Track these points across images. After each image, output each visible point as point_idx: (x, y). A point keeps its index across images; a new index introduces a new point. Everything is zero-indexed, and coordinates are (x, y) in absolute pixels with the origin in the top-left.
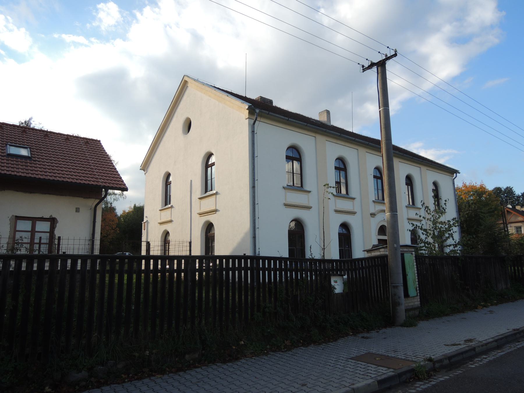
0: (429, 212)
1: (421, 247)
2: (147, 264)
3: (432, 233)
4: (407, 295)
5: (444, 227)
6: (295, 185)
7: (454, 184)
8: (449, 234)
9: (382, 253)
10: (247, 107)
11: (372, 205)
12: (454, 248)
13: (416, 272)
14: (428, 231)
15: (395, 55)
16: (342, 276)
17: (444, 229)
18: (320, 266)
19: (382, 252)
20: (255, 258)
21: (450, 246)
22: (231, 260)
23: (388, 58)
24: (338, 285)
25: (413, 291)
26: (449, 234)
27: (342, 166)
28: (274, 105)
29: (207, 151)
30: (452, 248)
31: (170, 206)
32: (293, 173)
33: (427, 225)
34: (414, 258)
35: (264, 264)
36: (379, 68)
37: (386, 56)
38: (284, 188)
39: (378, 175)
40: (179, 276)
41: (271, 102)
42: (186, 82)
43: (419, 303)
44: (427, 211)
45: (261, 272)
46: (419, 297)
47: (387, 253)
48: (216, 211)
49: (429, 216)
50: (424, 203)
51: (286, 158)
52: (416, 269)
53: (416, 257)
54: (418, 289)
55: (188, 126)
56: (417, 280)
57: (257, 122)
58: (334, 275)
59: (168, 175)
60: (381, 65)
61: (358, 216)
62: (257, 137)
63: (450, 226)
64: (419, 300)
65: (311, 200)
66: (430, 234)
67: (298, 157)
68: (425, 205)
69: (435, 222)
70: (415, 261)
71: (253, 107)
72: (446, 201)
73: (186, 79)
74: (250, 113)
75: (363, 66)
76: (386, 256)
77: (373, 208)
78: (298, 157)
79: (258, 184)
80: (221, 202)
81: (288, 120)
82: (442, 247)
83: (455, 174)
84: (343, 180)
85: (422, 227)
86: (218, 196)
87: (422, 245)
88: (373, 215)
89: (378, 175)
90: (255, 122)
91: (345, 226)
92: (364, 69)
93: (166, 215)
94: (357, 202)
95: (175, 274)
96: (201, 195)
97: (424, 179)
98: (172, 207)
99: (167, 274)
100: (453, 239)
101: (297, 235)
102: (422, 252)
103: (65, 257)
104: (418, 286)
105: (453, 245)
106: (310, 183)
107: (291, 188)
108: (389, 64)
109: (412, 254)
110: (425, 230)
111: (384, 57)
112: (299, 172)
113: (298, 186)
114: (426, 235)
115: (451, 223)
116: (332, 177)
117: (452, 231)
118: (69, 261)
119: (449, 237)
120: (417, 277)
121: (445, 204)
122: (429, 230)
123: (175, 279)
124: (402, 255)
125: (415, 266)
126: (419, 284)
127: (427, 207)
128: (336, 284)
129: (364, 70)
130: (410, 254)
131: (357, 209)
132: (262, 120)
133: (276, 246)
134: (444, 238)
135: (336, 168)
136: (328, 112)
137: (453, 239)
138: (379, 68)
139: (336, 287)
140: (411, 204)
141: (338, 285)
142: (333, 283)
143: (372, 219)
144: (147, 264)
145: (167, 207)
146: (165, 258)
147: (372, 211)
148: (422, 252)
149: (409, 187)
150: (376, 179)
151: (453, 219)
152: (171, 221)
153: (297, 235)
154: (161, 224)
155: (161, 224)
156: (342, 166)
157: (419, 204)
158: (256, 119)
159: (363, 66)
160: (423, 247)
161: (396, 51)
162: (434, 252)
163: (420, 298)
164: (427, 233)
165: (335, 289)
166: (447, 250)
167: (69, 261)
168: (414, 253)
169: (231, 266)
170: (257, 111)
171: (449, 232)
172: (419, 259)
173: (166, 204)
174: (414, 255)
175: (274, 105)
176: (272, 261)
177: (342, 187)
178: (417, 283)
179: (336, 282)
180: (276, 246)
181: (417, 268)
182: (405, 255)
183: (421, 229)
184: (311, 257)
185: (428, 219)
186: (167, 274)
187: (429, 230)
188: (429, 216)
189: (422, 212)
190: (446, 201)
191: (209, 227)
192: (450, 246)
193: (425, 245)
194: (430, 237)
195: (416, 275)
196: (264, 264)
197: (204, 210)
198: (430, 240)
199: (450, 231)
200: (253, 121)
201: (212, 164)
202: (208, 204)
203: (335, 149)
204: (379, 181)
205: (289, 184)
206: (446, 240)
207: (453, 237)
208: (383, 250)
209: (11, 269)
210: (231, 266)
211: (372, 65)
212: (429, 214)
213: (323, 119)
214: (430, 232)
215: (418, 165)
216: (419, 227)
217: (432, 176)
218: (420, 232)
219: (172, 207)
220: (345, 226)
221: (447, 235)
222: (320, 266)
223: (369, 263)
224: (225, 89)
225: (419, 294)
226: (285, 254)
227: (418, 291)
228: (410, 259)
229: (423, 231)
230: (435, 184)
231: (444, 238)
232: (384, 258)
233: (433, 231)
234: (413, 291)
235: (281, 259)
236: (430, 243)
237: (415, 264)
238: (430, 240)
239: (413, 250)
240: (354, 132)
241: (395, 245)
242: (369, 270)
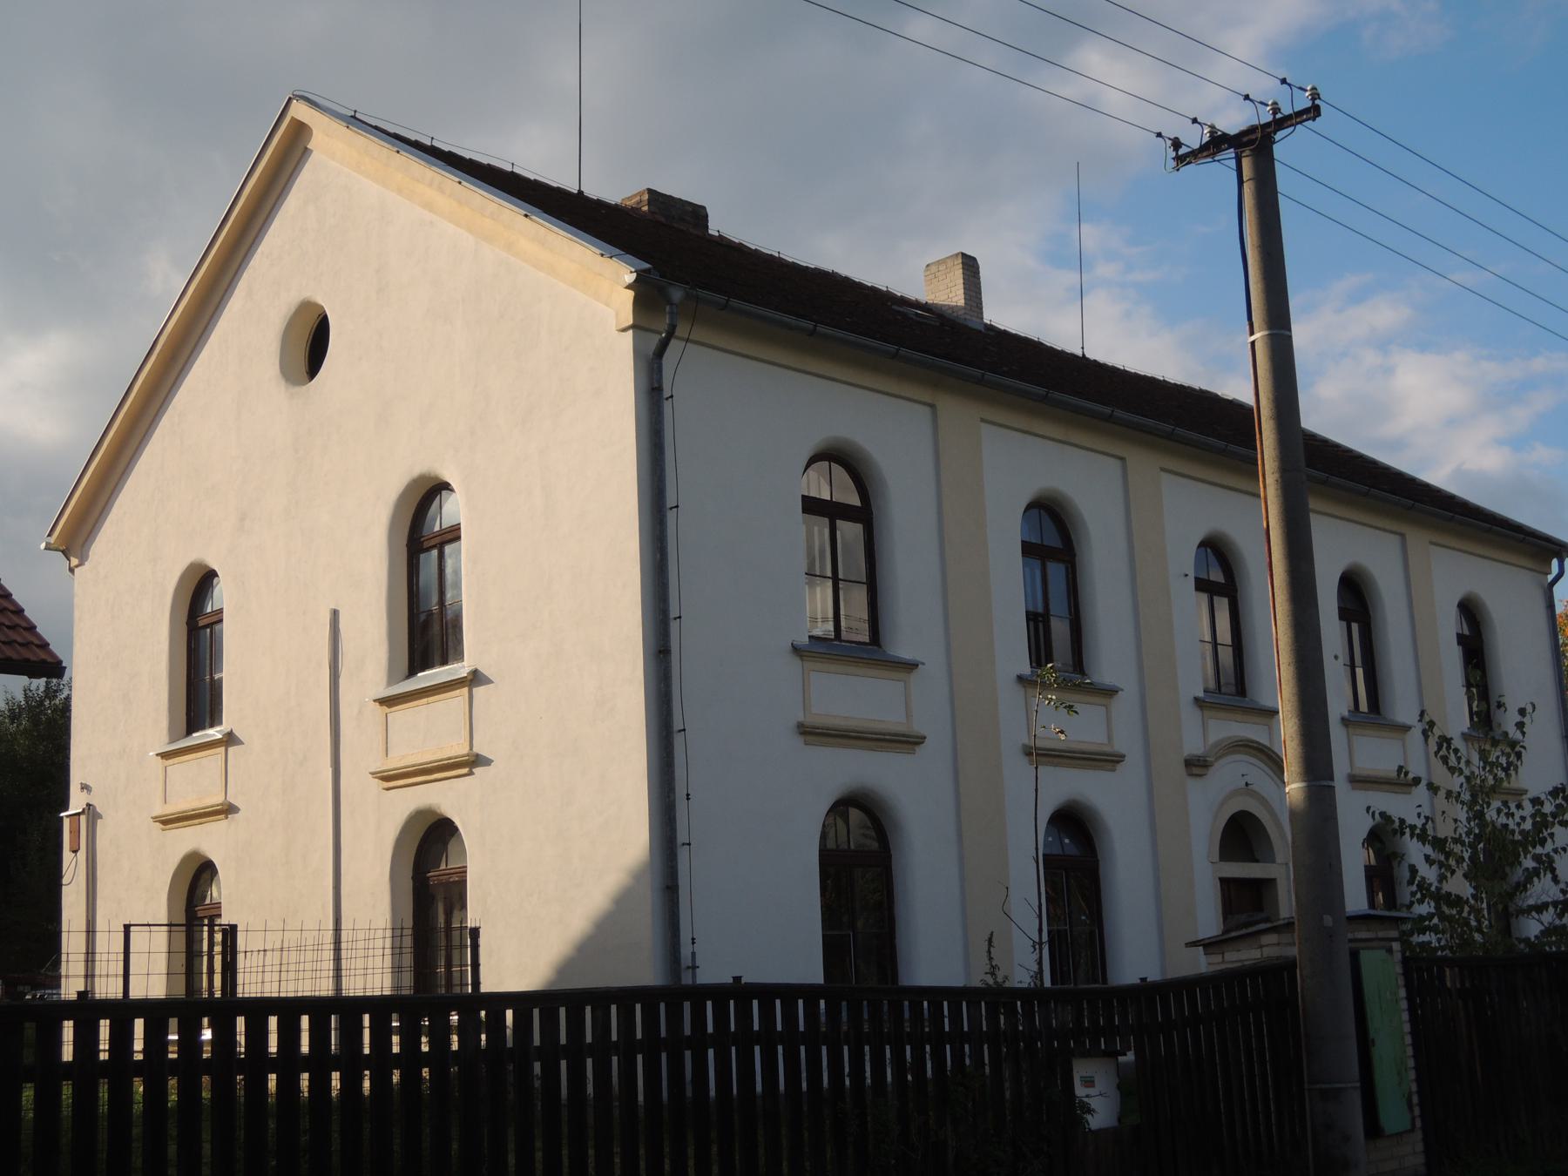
0: (1453, 761)
1: (1421, 918)
2: (87, 1039)
3: (1466, 856)
4: (1373, 1129)
5: (1521, 820)
6: (844, 635)
7: (1551, 606)
8: (1537, 858)
9: (1268, 952)
10: (630, 278)
11: (1190, 718)
12: (1561, 916)
13: (1407, 1028)
14: (1450, 846)
15: (1314, 112)
16: (1112, 1054)
17: (1517, 837)
18: (1029, 1014)
19: (1268, 949)
20: (677, 992)
21: (1540, 908)
22: (687, 1005)
23: (1282, 122)
24: (1098, 1096)
25: (1395, 1113)
26: (1537, 858)
27: (1053, 537)
28: (713, 231)
29: (417, 471)
30: (1548, 916)
31: (214, 733)
32: (835, 579)
33: (1453, 820)
34: (1399, 969)
35: (767, 1014)
36: (1246, 163)
37: (1276, 110)
38: (797, 650)
39: (1217, 576)
40: (156, 1093)
41: (698, 215)
42: (300, 131)
43: (1421, 1159)
44: (1445, 760)
45: (688, 1054)
46: (1419, 1135)
47: (1293, 951)
48: (475, 762)
49: (1456, 782)
50: (1432, 724)
51: (805, 510)
52: (1405, 1016)
53: (1405, 962)
54: (1415, 1099)
55: (312, 344)
56: (1411, 1063)
57: (675, 346)
58: (1086, 1054)
59: (201, 583)
60: (1254, 147)
61: (1132, 771)
62: (679, 416)
63: (1541, 823)
64: (1420, 1147)
65: (919, 703)
66: (1460, 860)
67: (855, 500)
68: (1427, 719)
69: (1478, 795)
70: (1401, 981)
71: (655, 276)
72: (1522, 712)
73: (300, 111)
74: (641, 304)
75: (1177, 144)
76: (1289, 966)
77: (1196, 734)
78: (855, 500)
79: (685, 638)
80: (498, 719)
81: (812, 333)
82: (1506, 916)
83: (1555, 562)
84: (1059, 606)
85: (1424, 829)
86: (479, 691)
87: (1425, 909)
88: (1196, 765)
89: (1217, 576)
90: (664, 345)
91: (1073, 823)
92: (1183, 157)
93: (197, 780)
94: (1125, 706)
95: (273, 1077)
96: (391, 681)
97: (1422, 588)
98: (230, 739)
99: (454, 1069)
100: (1555, 880)
101: (859, 868)
102: (1425, 938)
103: (259, 1009)
104: (1414, 1087)
105: (1555, 904)
106: (914, 628)
107: (827, 649)
108: (1286, 147)
109: (1390, 951)
110: (1439, 844)
111: (1266, 117)
112: (861, 571)
113: (865, 647)
114: (1441, 865)
115: (1548, 808)
116: (1008, 586)
117: (1549, 847)
118: (104, 1027)
119: (1536, 872)
120: (1410, 1051)
121: (1520, 726)
122: (1456, 841)
123: (138, 1108)
124: (1354, 956)
125: (1404, 1004)
126: (1418, 1080)
127: (1445, 741)
128: (1090, 1091)
129: (1181, 160)
130: (1382, 954)
131: (1126, 740)
132: (697, 334)
133: (770, 933)
134: (1517, 875)
135: (1028, 549)
136: (970, 266)
137: (1555, 880)
138: (1246, 163)
139: (1094, 1103)
140: (1364, 706)
141: (1098, 1096)
142: (1080, 1091)
143: (1193, 785)
144: (87, 1039)
145: (198, 737)
146: (204, 995)
147: (1194, 745)
148: (1425, 938)
149: (1355, 626)
150: (1204, 597)
151: (1555, 793)
152: (228, 810)
153: (859, 868)
154: (167, 821)
155: (167, 821)
156: (1053, 537)
157: (1403, 707)
158: (671, 334)
159: (1177, 144)
160: (1430, 916)
161: (1315, 95)
162: (1477, 937)
163: (1425, 1140)
164: (1448, 855)
165: (1090, 1111)
166: (1532, 928)
167: (104, 1027)
168: (1396, 946)
169: (687, 1031)
170: (677, 294)
171: (1539, 850)
172: (1418, 968)
173: (191, 727)
174: (1398, 956)
175: (713, 231)
176: (709, 1004)
177: (1058, 644)
178: (1412, 1075)
179: (1089, 1082)
180: (770, 933)
181: (1412, 1009)
182: (1367, 957)
183: (1423, 837)
184: (991, 981)
185: (1449, 794)
186: (454, 1069)
187: (1456, 841)
188: (1456, 782)
189: (1416, 756)
190: (1522, 712)
191: (432, 840)
192: (1540, 908)
193: (1437, 907)
194: (1459, 874)
195: (1408, 1040)
196: (767, 1014)
197: (401, 758)
198: (1459, 886)
199: (1543, 842)
200: (654, 341)
201: (443, 532)
202: (431, 729)
203: (1020, 461)
204: (1222, 604)
205: (818, 632)
206: (1522, 887)
207: (1553, 870)
208: (1271, 938)
209: (205, 1056)
210: (687, 1031)
211: (1217, 143)
212: (1452, 770)
213: (948, 293)
214: (1457, 848)
215: (1395, 527)
216: (1413, 827)
217: (1455, 572)
218: (1415, 852)
219: (230, 739)
220: (1073, 823)
221: (1529, 863)
222: (1029, 1014)
223: (1193, 1004)
224: (392, 129)
225: (1418, 1123)
226: (811, 971)
227: (1417, 1111)
228: (1383, 972)
229: (1428, 850)
230: (1470, 611)
231: (1517, 875)
232: (1278, 973)
233: (1473, 846)
234: (1395, 1113)
235: (790, 993)
236: (1458, 901)
237: (1403, 993)
238: (1459, 886)
239: (1394, 934)
240: (1091, 355)
241: (1328, 920)
242: (792, 1060)
